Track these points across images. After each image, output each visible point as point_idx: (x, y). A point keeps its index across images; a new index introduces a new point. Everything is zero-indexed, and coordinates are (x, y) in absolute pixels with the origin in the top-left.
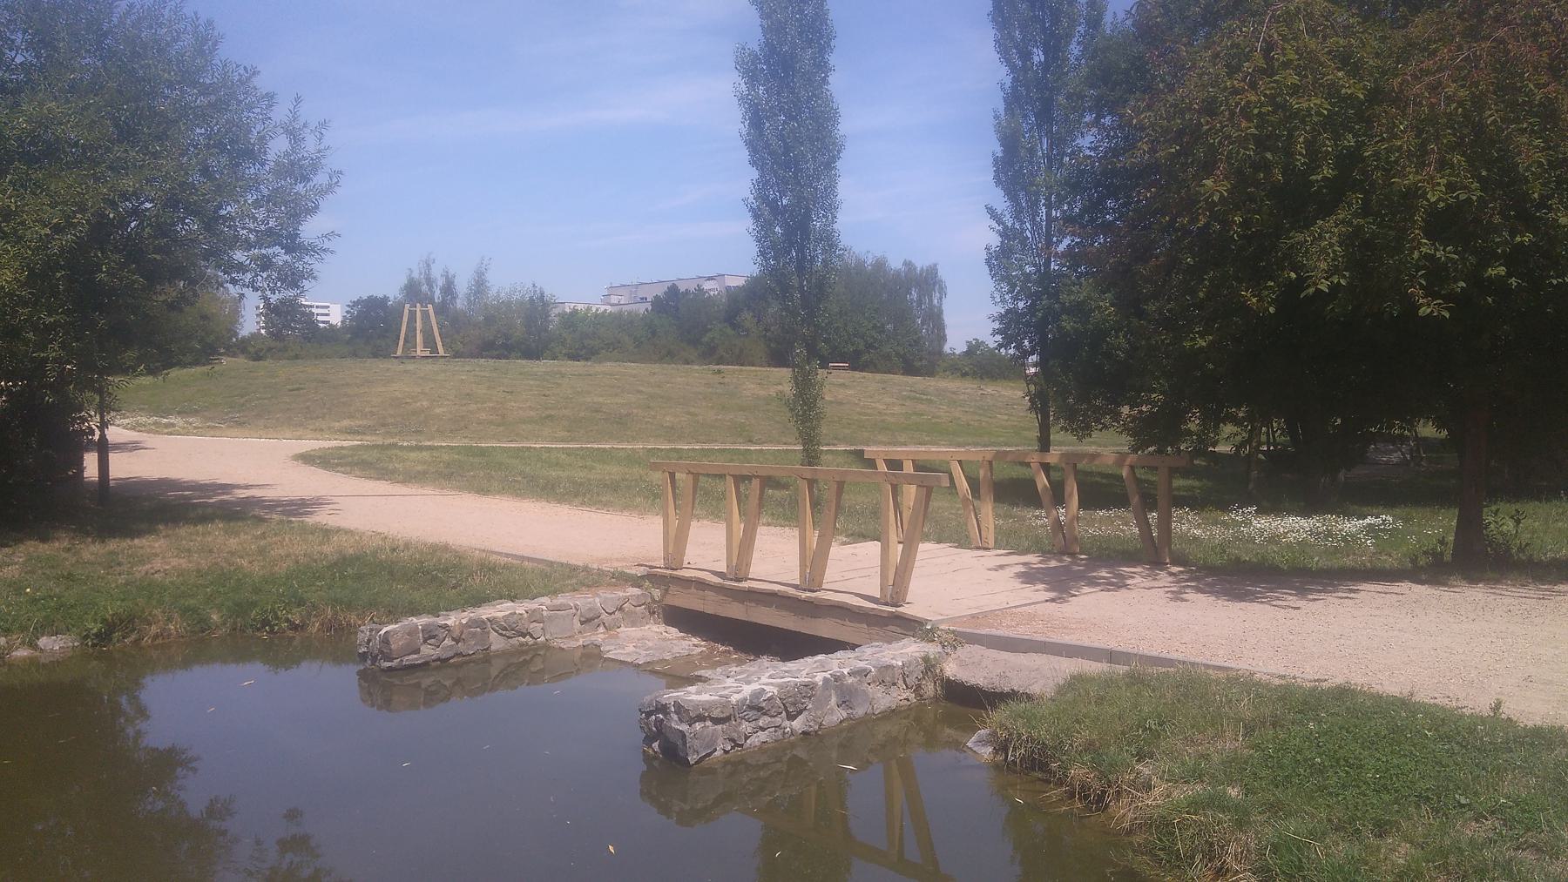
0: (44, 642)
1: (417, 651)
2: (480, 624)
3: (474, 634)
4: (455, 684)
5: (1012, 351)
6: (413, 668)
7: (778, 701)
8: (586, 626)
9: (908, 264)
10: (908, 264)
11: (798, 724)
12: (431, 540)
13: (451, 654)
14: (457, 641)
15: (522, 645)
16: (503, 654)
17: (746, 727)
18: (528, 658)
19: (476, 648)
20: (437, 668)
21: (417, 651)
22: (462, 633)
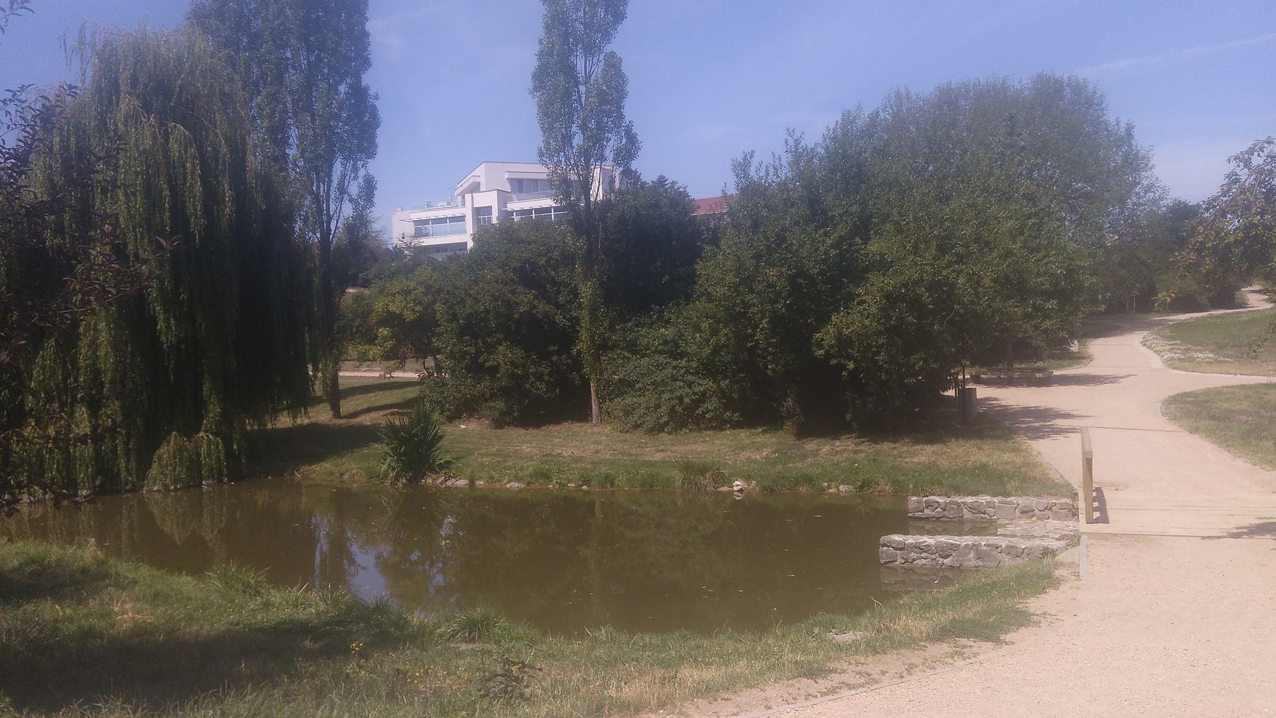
0: (841, 487)
1: (922, 511)
2: (958, 504)
3: (953, 509)
4: (943, 531)
5: (524, 331)
6: (919, 519)
7: (933, 548)
8: (1024, 515)
9: (662, 181)
10: (662, 181)
11: (947, 561)
12: (1242, 464)
13: (941, 516)
14: (944, 510)
15: (982, 518)
16: (971, 521)
17: (913, 555)
18: (987, 526)
19: (954, 515)
20: (932, 521)
21: (922, 511)
22: (946, 506)
